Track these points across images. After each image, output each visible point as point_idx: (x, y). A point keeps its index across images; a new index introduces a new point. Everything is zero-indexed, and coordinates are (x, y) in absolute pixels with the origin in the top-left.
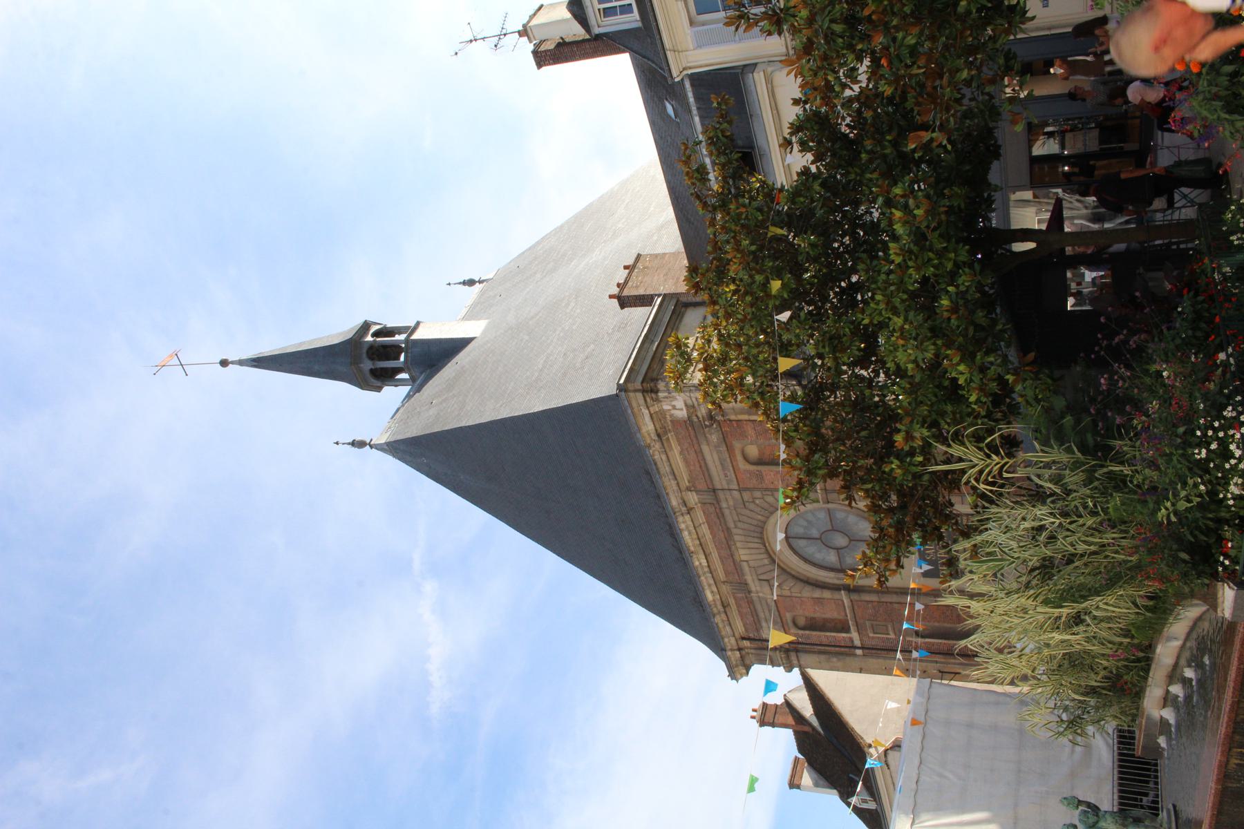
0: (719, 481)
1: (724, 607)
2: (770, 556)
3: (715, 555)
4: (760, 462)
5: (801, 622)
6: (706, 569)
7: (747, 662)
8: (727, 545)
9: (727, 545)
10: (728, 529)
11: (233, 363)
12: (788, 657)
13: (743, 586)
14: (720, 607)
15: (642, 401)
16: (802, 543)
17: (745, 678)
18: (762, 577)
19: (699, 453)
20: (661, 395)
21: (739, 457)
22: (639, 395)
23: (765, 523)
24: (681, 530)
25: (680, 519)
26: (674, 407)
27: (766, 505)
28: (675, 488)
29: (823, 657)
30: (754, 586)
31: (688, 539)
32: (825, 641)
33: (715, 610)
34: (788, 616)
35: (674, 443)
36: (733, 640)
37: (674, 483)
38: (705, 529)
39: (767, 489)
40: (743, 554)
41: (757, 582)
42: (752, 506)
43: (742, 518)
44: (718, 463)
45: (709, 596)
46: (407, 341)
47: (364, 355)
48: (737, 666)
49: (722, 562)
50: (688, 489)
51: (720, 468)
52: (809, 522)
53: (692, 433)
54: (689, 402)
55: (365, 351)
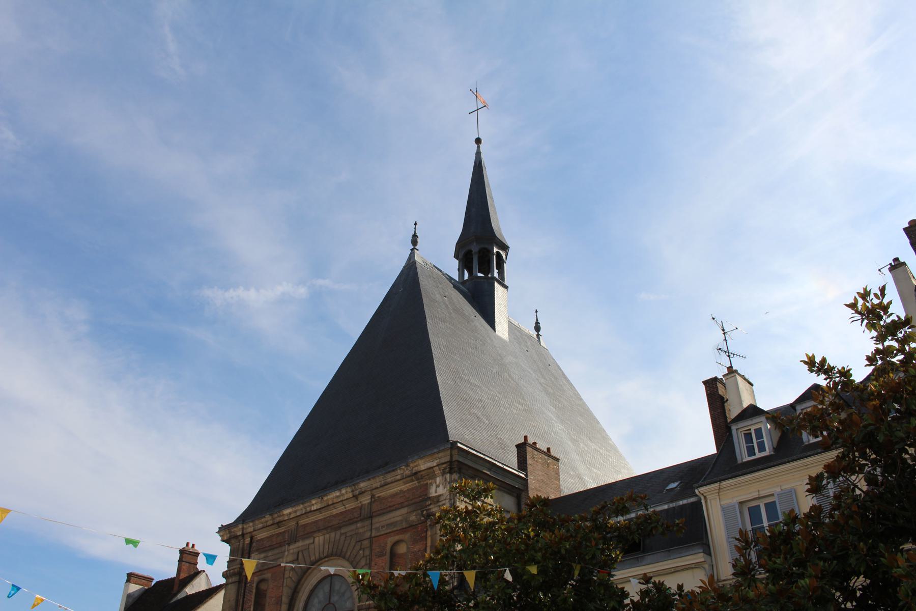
1: (278, 523)
3: (319, 516)
5: (263, 586)
6: (308, 509)
9: (327, 526)
10: (340, 528)
11: (478, 147)
15: (443, 460)
16: (327, 588)
18: (300, 554)
20: (448, 476)
21: (397, 538)
23: (344, 558)
24: (340, 490)
26: (438, 486)
28: (374, 486)
30: (294, 547)
31: (333, 495)
34: (268, 575)
36: (251, 529)
37: (378, 485)
38: (340, 509)
40: (319, 539)
41: (296, 550)
42: (358, 547)
44: (393, 520)
47: (483, 246)
48: (230, 532)
49: (314, 522)
50: (373, 496)
51: (389, 522)
54: (442, 498)
55: (486, 246)
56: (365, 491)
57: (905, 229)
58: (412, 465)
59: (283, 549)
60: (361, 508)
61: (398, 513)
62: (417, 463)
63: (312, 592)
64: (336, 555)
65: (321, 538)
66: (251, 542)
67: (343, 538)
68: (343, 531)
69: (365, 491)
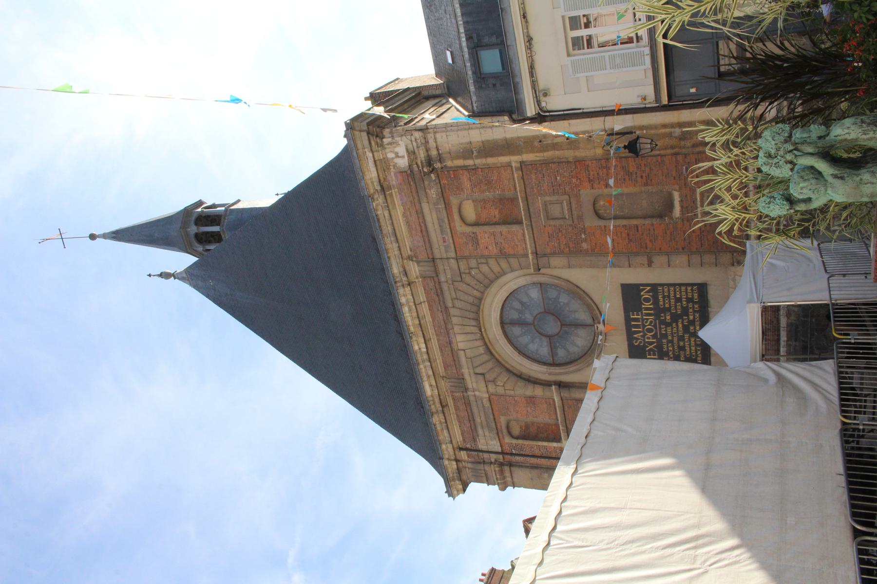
0: (439, 251)
1: (443, 407)
2: (485, 344)
3: (434, 343)
4: (476, 224)
5: (516, 431)
6: (425, 357)
7: (464, 477)
8: (445, 331)
9: (445, 331)
10: (446, 308)
11: (99, 236)
12: (502, 472)
13: (460, 383)
14: (438, 405)
15: (366, 143)
16: (517, 330)
17: (461, 495)
18: (479, 370)
19: (420, 213)
20: (386, 141)
21: (456, 217)
22: (364, 134)
23: (480, 300)
24: (402, 305)
25: (401, 291)
26: (397, 156)
27: (480, 277)
28: (397, 252)
29: (535, 472)
30: (470, 382)
31: (408, 315)
32: (537, 452)
33: (434, 410)
34: (503, 420)
35: (397, 201)
36: (451, 450)
37: (395, 245)
38: (425, 309)
39: (482, 257)
40: (461, 341)
41: (473, 377)
42: (467, 279)
43: (461, 295)
44: (437, 226)
45: (428, 390)
46: (226, 210)
47: (193, 222)
48: (454, 480)
49: (441, 350)
50: (410, 258)
51: (438, 231)
52: (523, 304)
53: (413, 186)
54: (410, 148)
55: (193, 219)
56: (403, 267)
57: (346, 123)
58: (372, 191)
59: (472, 399)
60: (424, 277)
61: (428, 218)
62: (369, 182)
63: (521, 352)
64: (477, 313)
65: (459, 338)
66: (466, 449)
67: (458, 304)
68: (450, 305)
69: (403, 267)
